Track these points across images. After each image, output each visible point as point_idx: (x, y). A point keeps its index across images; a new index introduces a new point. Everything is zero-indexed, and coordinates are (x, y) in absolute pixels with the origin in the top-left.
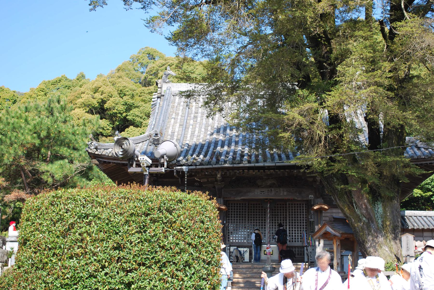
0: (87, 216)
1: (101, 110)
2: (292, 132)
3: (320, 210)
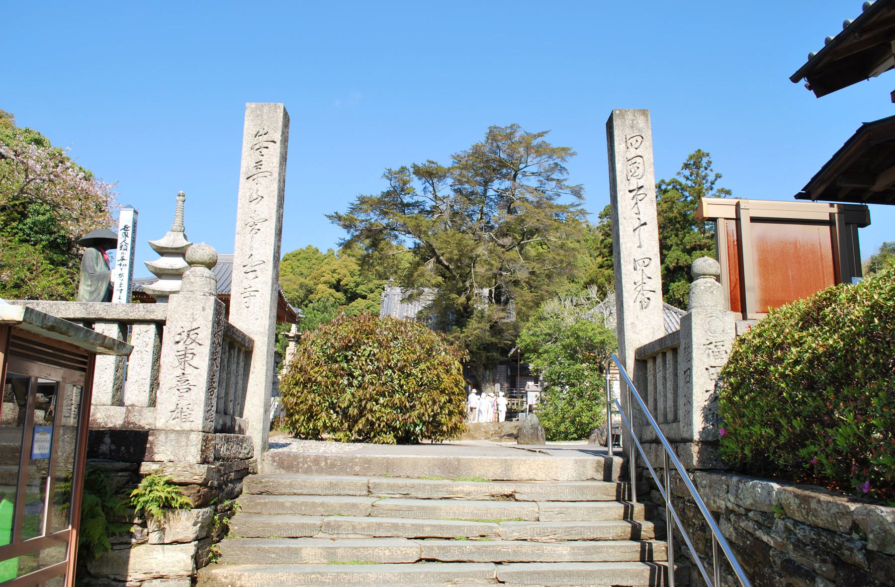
1: (337, 286)
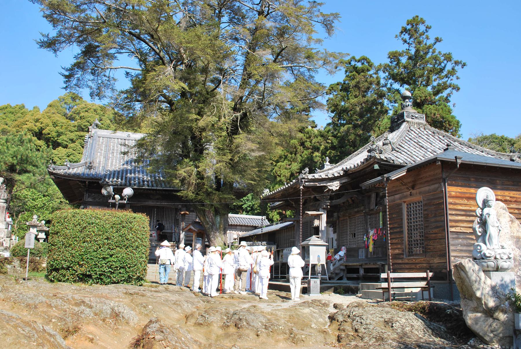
0: (93, 223)
1: (39, 135)
2: (180, 180)
3: (185, 214)
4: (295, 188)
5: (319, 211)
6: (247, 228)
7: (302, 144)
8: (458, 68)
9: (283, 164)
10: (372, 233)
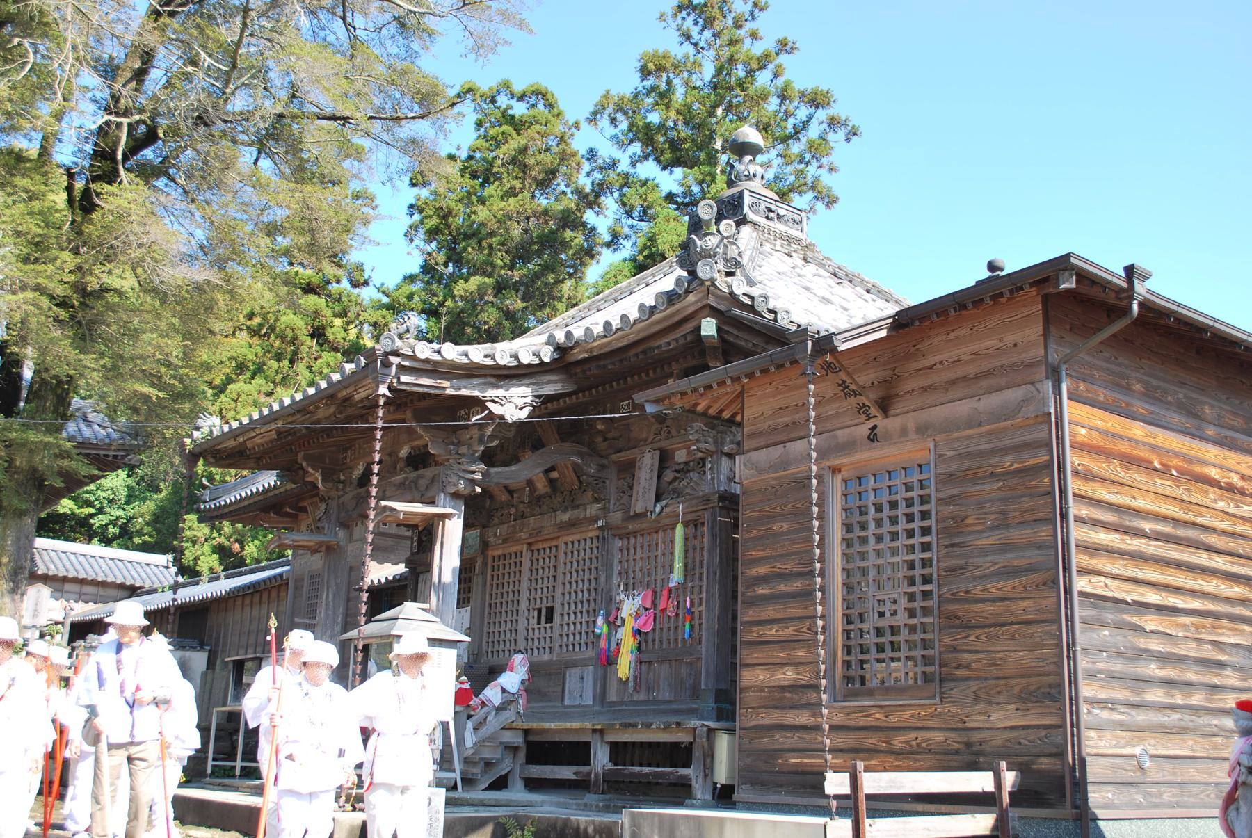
4: (347, 399)
5: (432, 503)
6: (101, 591)
7: (318, 333)
8: (836, 138)
9: (247, 387)
10: (629, 607)
